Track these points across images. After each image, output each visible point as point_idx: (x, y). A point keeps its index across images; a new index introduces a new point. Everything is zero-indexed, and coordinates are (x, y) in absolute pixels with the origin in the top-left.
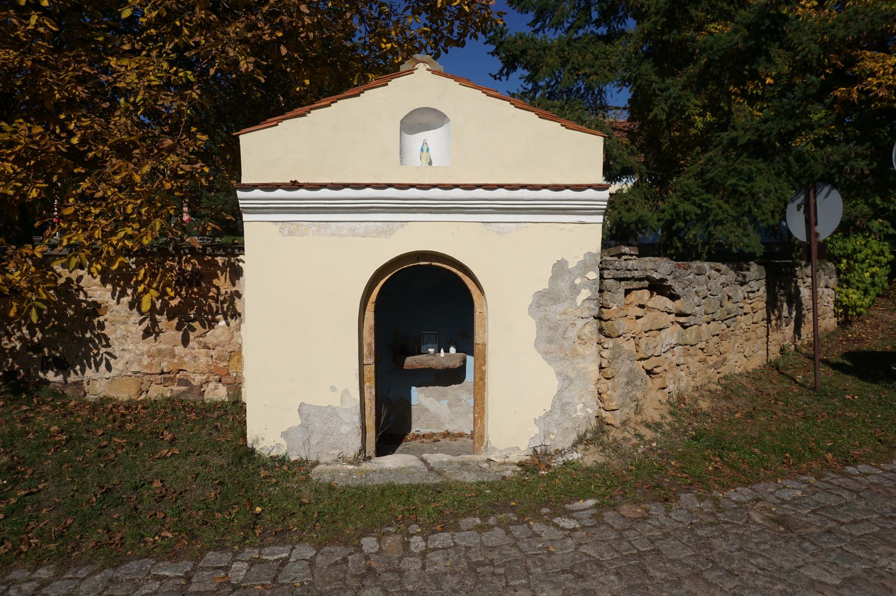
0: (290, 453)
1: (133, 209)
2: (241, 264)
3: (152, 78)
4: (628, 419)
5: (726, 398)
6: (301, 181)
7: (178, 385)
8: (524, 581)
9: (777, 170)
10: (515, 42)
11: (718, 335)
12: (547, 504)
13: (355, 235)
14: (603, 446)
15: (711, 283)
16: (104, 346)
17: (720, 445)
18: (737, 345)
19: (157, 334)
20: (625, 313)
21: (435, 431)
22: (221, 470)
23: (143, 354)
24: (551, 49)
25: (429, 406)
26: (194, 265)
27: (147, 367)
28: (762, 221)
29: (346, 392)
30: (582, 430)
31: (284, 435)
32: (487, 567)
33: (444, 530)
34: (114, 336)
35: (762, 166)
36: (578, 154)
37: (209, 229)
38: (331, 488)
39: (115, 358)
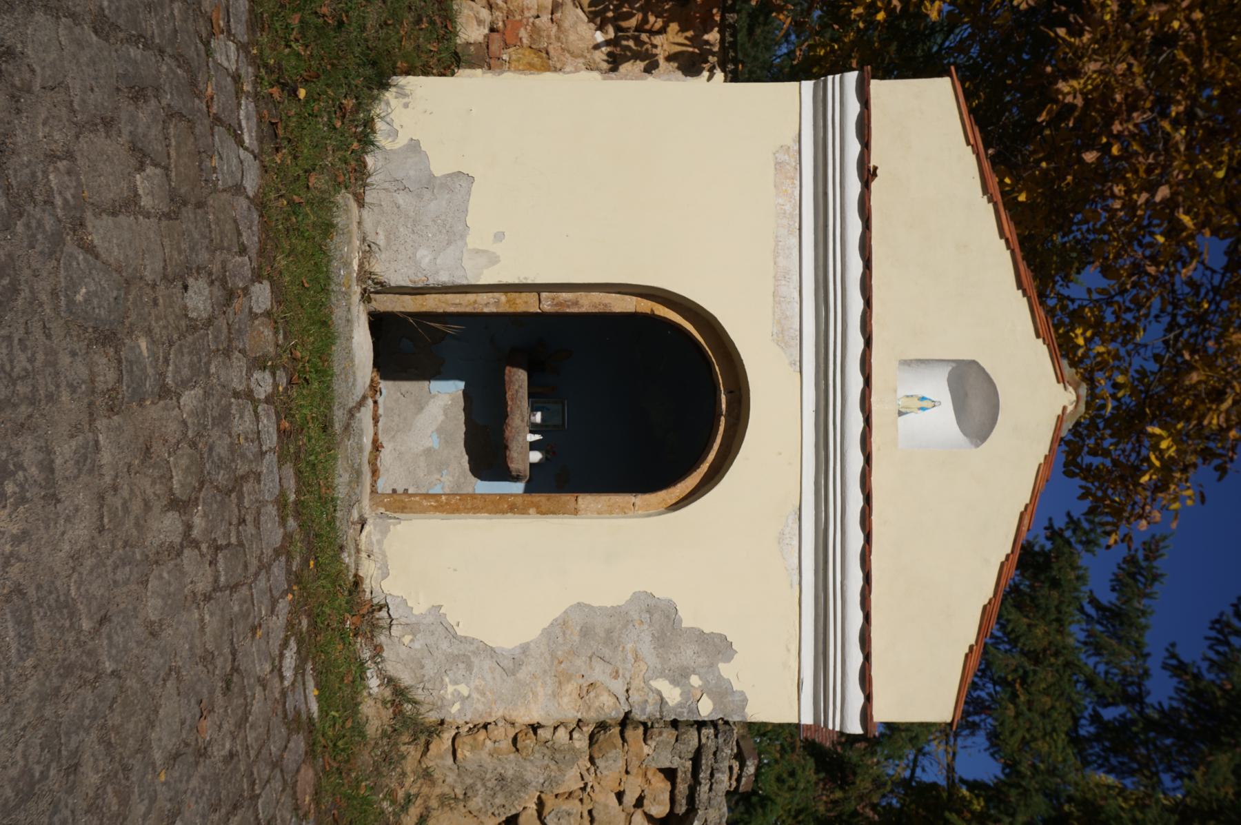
2: (706, 74)
4: (433, 783)
8: (222, 579)
10: (1074, 568)
12: (313, 625)
13: (776, 278)
14: (390, 735)
20: (633, 770)
24: (1060, 631)
29: (494, 260)
30: (419, 695)
31: (414, 146)
32: (236, 510)
33: (282, 433)
36: (921, 679)
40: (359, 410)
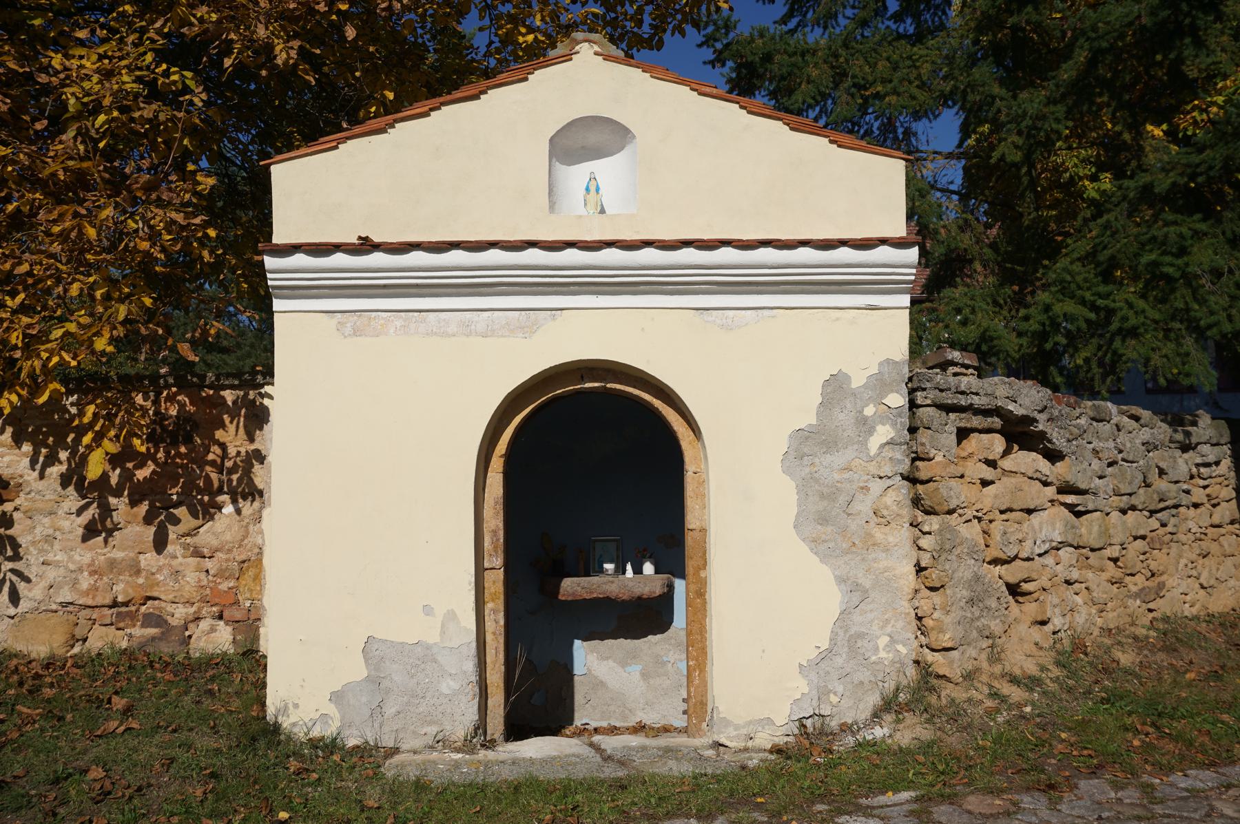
0: (345, 733)
1: (82, 290)
2: (266, 401)
3: (126, 78)
4: (978, 670)
5: (1170, 650)
6: (377, 239)
7: (143, 626)
9: (1229, 234)
10: (753, 40)
11: (1143, 538)
12: (822, 798)
15: (1122, 438)
16: (9, 559)
17: (1157, 712)
18: (1183, 561)
19: (110, 533)
20: (960, 471)
22: (216, 755)
23: (81, 570)
26: (182, 406)
27: (87, 593)
28: (1210, 327)
29: (451, 616)
30: (890, 686)
34: (30, 538)
35: (1203, 227)
36: (865, 191)
37: (212, 332)
38: (420, 786)
39: (28, 580)
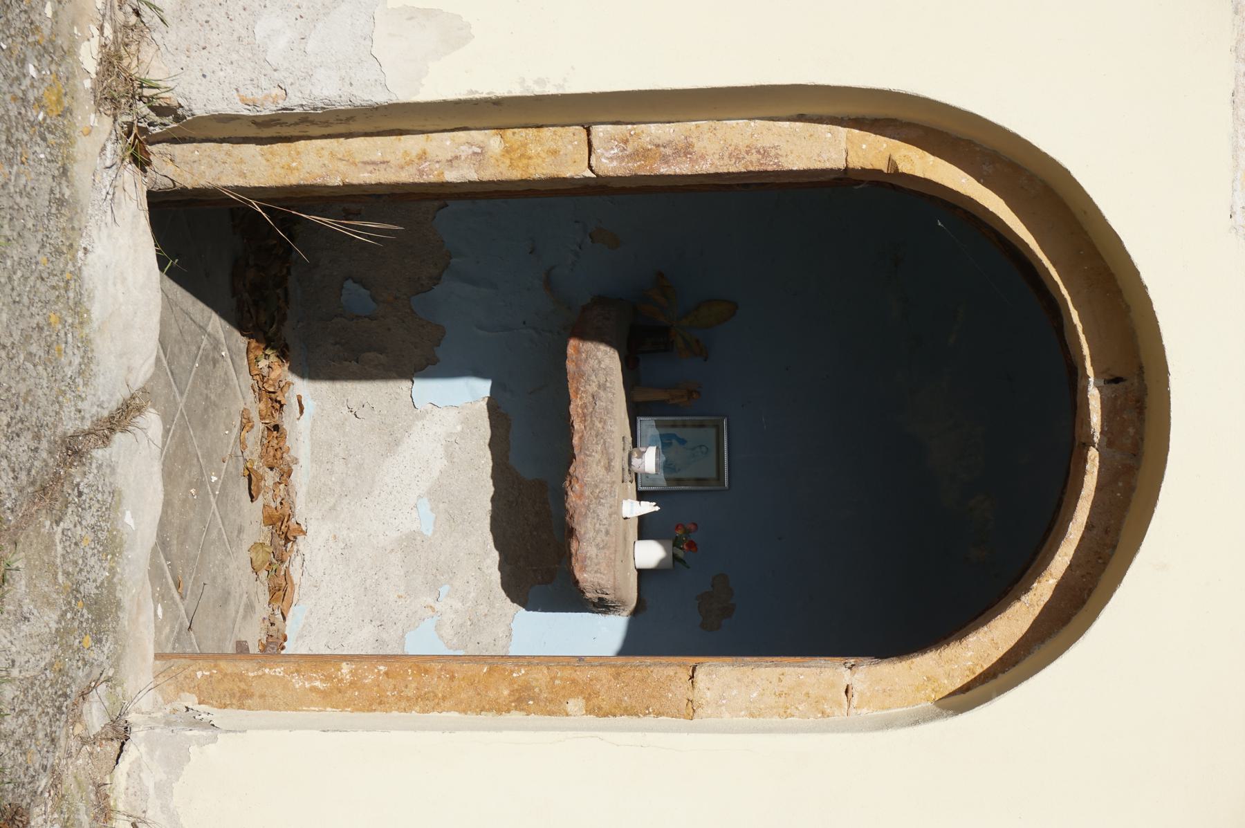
21: (301, 478)
25: (406, 454)
29: (455, 34)
40: (106, 440)
